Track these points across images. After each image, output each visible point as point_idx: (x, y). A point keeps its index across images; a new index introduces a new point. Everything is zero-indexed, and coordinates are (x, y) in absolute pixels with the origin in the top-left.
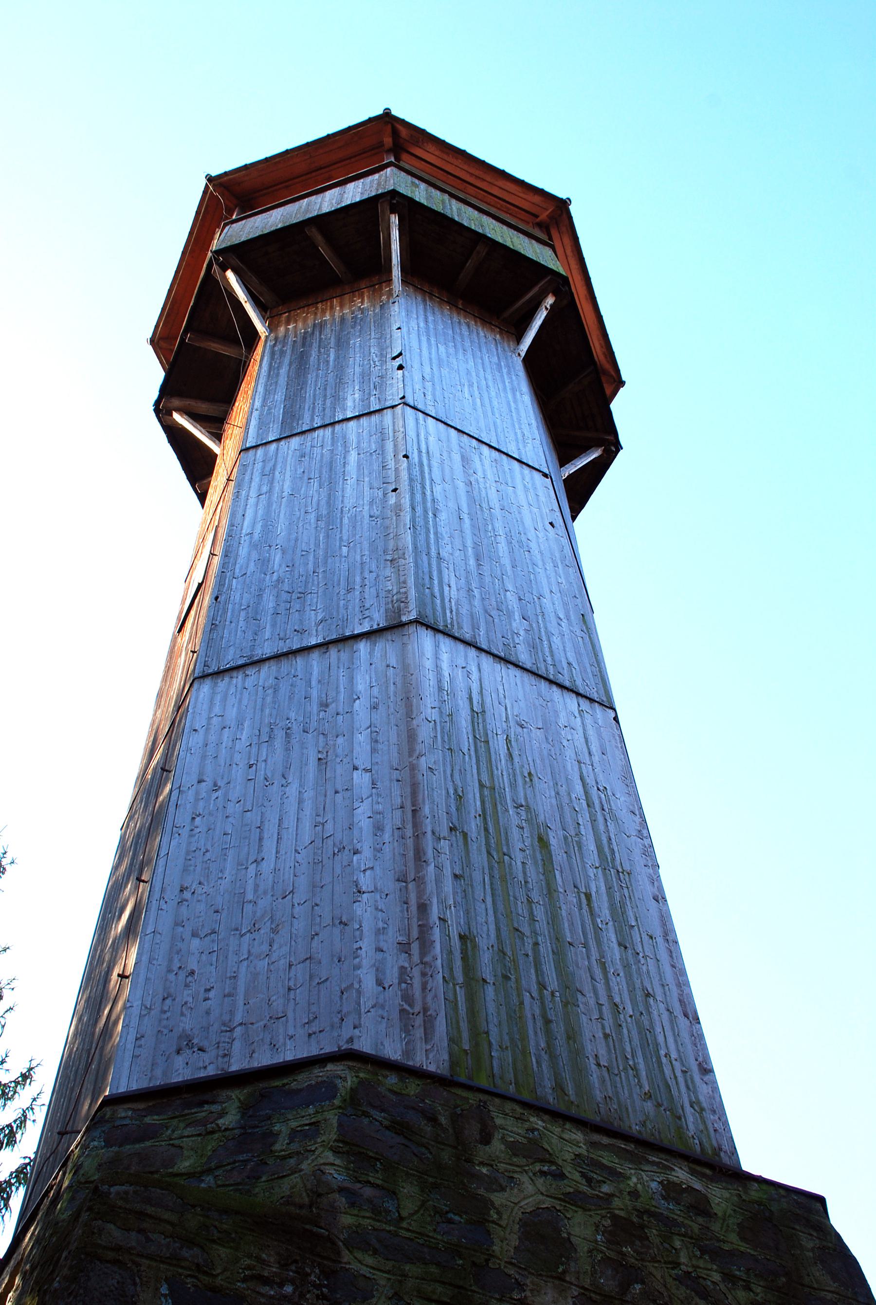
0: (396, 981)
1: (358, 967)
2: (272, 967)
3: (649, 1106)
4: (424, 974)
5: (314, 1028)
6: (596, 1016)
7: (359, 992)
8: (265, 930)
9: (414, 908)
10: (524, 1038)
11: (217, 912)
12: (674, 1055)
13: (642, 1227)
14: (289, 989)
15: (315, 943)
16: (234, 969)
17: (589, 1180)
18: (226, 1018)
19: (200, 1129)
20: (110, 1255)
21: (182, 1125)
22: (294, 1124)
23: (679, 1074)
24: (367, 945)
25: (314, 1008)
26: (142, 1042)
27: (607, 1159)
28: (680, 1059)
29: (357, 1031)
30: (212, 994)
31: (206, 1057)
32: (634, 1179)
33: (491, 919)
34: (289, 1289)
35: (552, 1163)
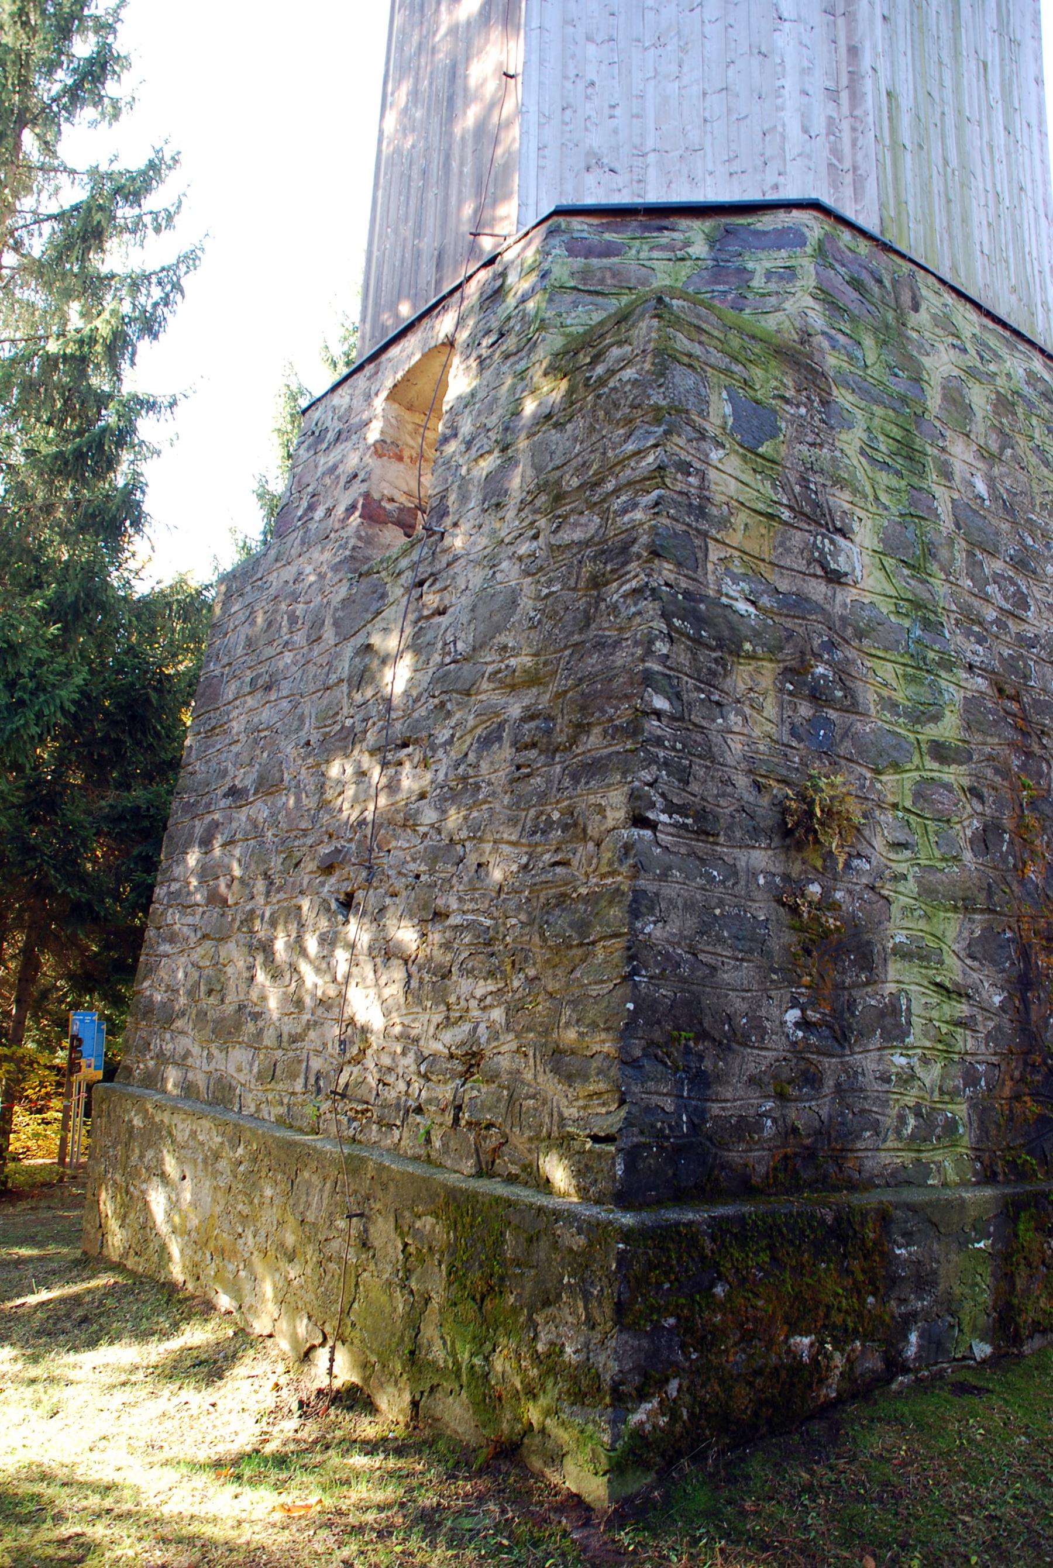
0: (824, 132)
1: (781, 108)
2: (683, 92)
3: (1014, 298)
4: (854, 129)
5: (736, 167)
6: (982, 203)
7: (783, 137)
8: (672, 46)
9: (843, 50)
10: (932, 215)
11: (613, 15)
12: (1034, 255)
13: (1013, 405)
14: (705, 121)
15: (731, 72)
16: (641, 87)
17: (982, 358)
18: (637, 141)
19: (669, 255)
20: (686, 360)
21: (646, 247)
22: (768, 265)
23: (1036, 273)
24: (790, 84)
25: (733, 146)
26: (546, 152)
27: (993, 342)
28: (1038, 259)
29: (782, 179)
30: (617, 112)
31: (619, 180)
32: (1009, 363)
33: (910, 77)
34: (803, 411)
35: (958, 337)
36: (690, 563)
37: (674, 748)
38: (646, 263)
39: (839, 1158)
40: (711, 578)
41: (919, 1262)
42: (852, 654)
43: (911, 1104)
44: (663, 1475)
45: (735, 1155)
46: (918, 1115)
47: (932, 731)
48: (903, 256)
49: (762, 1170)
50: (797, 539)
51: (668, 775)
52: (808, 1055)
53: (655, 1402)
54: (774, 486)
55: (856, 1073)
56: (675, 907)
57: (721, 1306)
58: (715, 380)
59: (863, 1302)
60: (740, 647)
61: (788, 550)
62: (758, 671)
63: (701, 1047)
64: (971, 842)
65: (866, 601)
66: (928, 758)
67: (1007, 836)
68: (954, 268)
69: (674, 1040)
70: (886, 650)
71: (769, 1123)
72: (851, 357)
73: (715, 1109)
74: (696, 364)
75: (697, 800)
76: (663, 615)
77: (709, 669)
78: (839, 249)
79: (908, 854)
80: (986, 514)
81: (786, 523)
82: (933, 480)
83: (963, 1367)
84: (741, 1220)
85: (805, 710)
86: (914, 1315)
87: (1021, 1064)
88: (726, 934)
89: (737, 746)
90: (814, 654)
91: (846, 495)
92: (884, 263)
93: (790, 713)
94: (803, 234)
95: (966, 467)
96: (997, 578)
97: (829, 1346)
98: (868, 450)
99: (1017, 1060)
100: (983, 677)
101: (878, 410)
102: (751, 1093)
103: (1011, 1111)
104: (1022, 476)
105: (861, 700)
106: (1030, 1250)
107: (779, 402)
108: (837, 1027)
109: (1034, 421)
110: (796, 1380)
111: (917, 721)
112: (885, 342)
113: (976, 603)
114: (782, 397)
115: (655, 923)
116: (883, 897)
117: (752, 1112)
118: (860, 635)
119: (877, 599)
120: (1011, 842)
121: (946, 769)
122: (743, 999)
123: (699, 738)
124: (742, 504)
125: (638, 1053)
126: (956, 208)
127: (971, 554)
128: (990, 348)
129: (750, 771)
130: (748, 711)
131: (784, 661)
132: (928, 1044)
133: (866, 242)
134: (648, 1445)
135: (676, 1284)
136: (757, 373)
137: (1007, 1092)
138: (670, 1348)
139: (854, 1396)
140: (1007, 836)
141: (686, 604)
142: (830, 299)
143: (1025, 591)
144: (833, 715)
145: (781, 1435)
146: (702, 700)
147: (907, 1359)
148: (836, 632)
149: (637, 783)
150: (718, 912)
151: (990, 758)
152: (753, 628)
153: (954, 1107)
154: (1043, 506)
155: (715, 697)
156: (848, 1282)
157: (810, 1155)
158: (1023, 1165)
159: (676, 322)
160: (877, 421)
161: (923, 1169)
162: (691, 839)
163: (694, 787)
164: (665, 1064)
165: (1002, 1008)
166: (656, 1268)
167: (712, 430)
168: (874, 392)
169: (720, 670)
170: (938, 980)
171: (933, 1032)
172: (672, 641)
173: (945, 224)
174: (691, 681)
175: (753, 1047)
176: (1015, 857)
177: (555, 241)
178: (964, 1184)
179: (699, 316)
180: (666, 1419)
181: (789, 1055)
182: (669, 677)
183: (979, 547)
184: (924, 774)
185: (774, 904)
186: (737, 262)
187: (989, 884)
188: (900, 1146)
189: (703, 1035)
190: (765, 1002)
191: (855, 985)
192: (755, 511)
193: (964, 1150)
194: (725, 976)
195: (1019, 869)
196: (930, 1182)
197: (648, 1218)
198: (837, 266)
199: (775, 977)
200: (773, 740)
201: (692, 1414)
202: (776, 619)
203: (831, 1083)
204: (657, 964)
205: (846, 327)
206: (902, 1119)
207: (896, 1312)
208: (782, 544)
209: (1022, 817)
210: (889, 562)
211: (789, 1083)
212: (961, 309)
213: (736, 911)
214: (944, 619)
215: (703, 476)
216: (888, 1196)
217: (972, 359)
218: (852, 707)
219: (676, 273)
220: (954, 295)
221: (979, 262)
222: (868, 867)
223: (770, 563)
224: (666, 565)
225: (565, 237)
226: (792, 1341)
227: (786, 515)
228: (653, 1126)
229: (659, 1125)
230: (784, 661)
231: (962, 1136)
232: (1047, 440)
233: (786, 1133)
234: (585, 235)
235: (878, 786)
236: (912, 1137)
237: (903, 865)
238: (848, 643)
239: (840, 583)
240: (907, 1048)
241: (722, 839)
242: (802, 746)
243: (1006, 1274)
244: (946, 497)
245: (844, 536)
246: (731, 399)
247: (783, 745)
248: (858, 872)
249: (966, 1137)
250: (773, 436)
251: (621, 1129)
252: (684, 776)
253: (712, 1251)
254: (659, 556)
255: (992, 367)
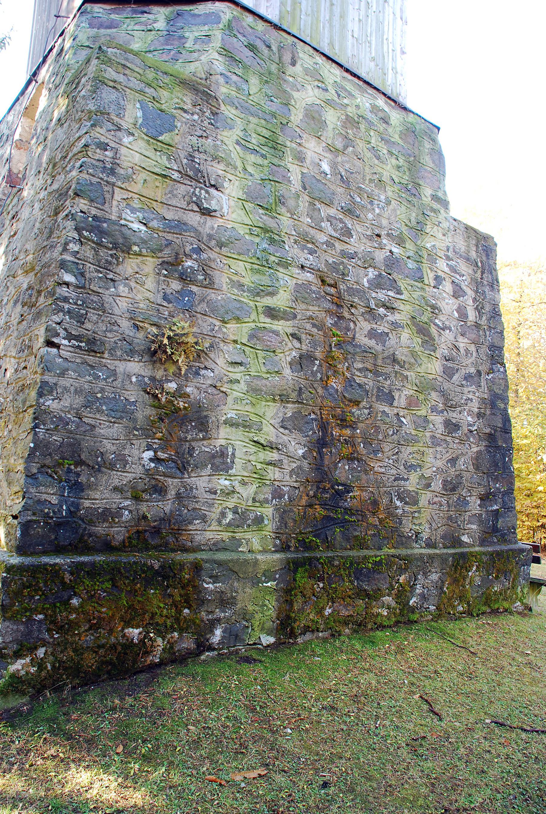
3: (372, 64)
10: (318, 11)
12: (390, 40)
17: (339, 95)
20: (112, 84)
21: (133, 23)
22: (197, 34)
23: (390, 51)
27: (349, 87)
32: (359, 100)
34: (196, 117)
36: (100, 200)
37: (76, 304)
38: (130, 32)
39: (177, 533)
40: (115, 209)
41: (222, 592)
42: (213, 255)
43: (231, 507)
44: (34, 698)
45: (100, 529)
46: (235, 512)
47: (268, 301)
48: (289, 33)
49: (121, 538)
50: (182, 189)
51: (70, 318)
52: (158, 477)
53: (28, 660)
54: (169, 159)
55: (192, 488)
56: (69, 391)
57: (75, 610)
58: (132, 97)
59: (180, 612)
60: (130, 248)
61: (175, 196)
62: (143, 262)
63: (79, 469)
64: (290, 363)
65: (229, 227)
66: (263, 316)
67: (317, 362)
68: (331, 44)
69: (60, 465)
70: (239, 254)
71: (127, 513)
72: (239, 89)
73: (87, 503)
74: (118, 87)
75: (89, 333)
76: (76, 229)
77: (107, 260)
78: (242, 27)
79: (242, 368)
80: (327, 182)
81: (175, 180)
82: (289, 161)
83: (253, 649)
84: (93, 564)
85: (176, 285)
86: (219, 620)
87: (315, 488)
88: (104, 408)
89: (123, 304)
90: (186, 255)
91: (222, 166)
92: (274, 37)
93: (164, 287)
94: (220, 17)
95: (316, 155)
96: (329, 219)
97: (152, 635)
98: (243, 142)
99: (312, 486)
100: (310, 273)
101: (254, 120)
102: (114, 495)
103: (305, 513)
104: (358, 163)
105: (217, 281)
106: (305, 588)
107: (179, 111)
108: (179, 462)
109: (372, 133)
110: (128, 652)
111: (258, 294)
112: (267, 82)
113: (312, 232)
114: (182, 109)
115: (53, 400)
116: (222, 392)
117: (114, 506)
118: (221, 245)
119: (236, 225)
120: (320, 365)
121: (276, 322)
122: (113, 444)
123: (95, 299)
124: (144, 168)
125: (35, 471)
126: (337, 10)
127: (312, 204)
128: (346, 90)
129: (131, 318)
130: (133, 284)
131: (162, 257)
132: (246, 474)
133: (263, 23)
134: (23, 682)
135: (43, 597)
136: (164, 94)
137: (303, 502)
138: (39, 631)
139: (173, 661)
140: (317, 362)
141: (94, 223)
142: (230, 55)
143: (350, 227)
144: (194, 288)
145: (117, 680)
146: (100, 278)
147: (213, 643)
148: (203, 243)
149: (50, 323)
150: (99, 395)
151: (310, 318)
152: (142, 238)
153: (263, 509)
154: (371, 181)
155: (110, 276)
156: (170, 601)
157: (157, 531)
158: (310, 542)
159: (109, 62)
160: (251, 126)
161: (236, 543)
162: (85, 355)
163: (88, 325)
164: (53, 477)
165: (303, 457)
166: (28, 588)
167: (125, 126)
168: (252, 109)
169: (114, 261)
170: (255, 439)
171: (250, 468)
172: (82, 243)
173: (327, 18)
174: (92, 266)
175: (117, 471)
176: (322, 374)
177: (84, 18)
178: (264, 551)
179: (127, 59)
180: (35, 669)
181: (144, 476)
182: (77, 264)
183: (319, 201)
184: (259, 325)
185: (142, 393)
186: (180, 32)
187: (300, 389)
188: (220, 529)
189: (80, 463)
190: (128, 446)
191: (193, 440)
192: (153, 173)
193: (268, 533)
194: (101, 431)
195: (325, 382)
196: (240, 549)
197: (28, 560)
198: (239, 36)
199: (136, 433)
200: (150, 302)
201: (53, 666)
202: (160, 234)
203: (173, 493)
204: (53, 422)
205: (239, 72)
206: (223, 515)
207: (205, 618)
208: (171, 192)
209: (331, 351)
210: (249, 206)
211: (143, 492)
212: (328, 67)
213: (113, 395)
214: (286, 239)
215: (116, 152)
216: (200, 556)
217: (332, 94)
218: (210, 284)
219: (146, 39)
220: (324, 58)
221: (350, 42)
222: (212, 375)
223: (161, 202)
224: (82, 201)
225: (89, 16)
226: (126, 631)
227: (176, 176)
228: (42, 511)
229: (46, 510)
230: (162, 257)
231: (266, 525)
232: (380, 144)
233: (139, 519)
234: (100, 15)
235: (224, 330)
236: (229, 525)
237: (238, 374)
238: (211, 249)
239: (211, 216)
240: (230, 476)
241: (106, 355)
242: (170, 305)
243: (287, 601)
244: (298, 171)
245: (217, 189)
246: (142, 108)
247: (157, 304)
248: (204, 377)
249: (269, 526)
250: (171, 131)
251: (20, 512)
252: (81, 320)
253: (71, 581)
254: (78, 195)
255: (346, 101)
